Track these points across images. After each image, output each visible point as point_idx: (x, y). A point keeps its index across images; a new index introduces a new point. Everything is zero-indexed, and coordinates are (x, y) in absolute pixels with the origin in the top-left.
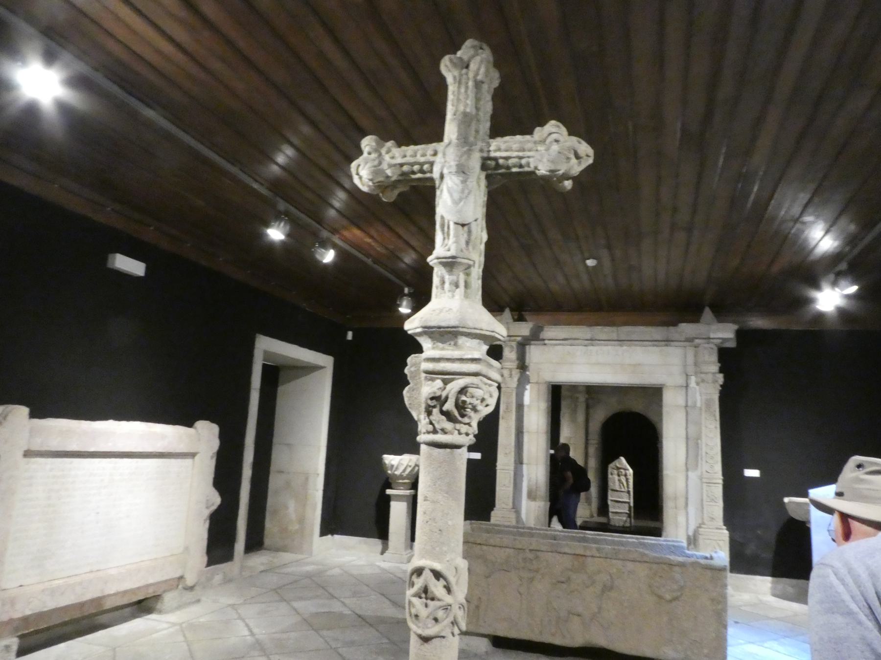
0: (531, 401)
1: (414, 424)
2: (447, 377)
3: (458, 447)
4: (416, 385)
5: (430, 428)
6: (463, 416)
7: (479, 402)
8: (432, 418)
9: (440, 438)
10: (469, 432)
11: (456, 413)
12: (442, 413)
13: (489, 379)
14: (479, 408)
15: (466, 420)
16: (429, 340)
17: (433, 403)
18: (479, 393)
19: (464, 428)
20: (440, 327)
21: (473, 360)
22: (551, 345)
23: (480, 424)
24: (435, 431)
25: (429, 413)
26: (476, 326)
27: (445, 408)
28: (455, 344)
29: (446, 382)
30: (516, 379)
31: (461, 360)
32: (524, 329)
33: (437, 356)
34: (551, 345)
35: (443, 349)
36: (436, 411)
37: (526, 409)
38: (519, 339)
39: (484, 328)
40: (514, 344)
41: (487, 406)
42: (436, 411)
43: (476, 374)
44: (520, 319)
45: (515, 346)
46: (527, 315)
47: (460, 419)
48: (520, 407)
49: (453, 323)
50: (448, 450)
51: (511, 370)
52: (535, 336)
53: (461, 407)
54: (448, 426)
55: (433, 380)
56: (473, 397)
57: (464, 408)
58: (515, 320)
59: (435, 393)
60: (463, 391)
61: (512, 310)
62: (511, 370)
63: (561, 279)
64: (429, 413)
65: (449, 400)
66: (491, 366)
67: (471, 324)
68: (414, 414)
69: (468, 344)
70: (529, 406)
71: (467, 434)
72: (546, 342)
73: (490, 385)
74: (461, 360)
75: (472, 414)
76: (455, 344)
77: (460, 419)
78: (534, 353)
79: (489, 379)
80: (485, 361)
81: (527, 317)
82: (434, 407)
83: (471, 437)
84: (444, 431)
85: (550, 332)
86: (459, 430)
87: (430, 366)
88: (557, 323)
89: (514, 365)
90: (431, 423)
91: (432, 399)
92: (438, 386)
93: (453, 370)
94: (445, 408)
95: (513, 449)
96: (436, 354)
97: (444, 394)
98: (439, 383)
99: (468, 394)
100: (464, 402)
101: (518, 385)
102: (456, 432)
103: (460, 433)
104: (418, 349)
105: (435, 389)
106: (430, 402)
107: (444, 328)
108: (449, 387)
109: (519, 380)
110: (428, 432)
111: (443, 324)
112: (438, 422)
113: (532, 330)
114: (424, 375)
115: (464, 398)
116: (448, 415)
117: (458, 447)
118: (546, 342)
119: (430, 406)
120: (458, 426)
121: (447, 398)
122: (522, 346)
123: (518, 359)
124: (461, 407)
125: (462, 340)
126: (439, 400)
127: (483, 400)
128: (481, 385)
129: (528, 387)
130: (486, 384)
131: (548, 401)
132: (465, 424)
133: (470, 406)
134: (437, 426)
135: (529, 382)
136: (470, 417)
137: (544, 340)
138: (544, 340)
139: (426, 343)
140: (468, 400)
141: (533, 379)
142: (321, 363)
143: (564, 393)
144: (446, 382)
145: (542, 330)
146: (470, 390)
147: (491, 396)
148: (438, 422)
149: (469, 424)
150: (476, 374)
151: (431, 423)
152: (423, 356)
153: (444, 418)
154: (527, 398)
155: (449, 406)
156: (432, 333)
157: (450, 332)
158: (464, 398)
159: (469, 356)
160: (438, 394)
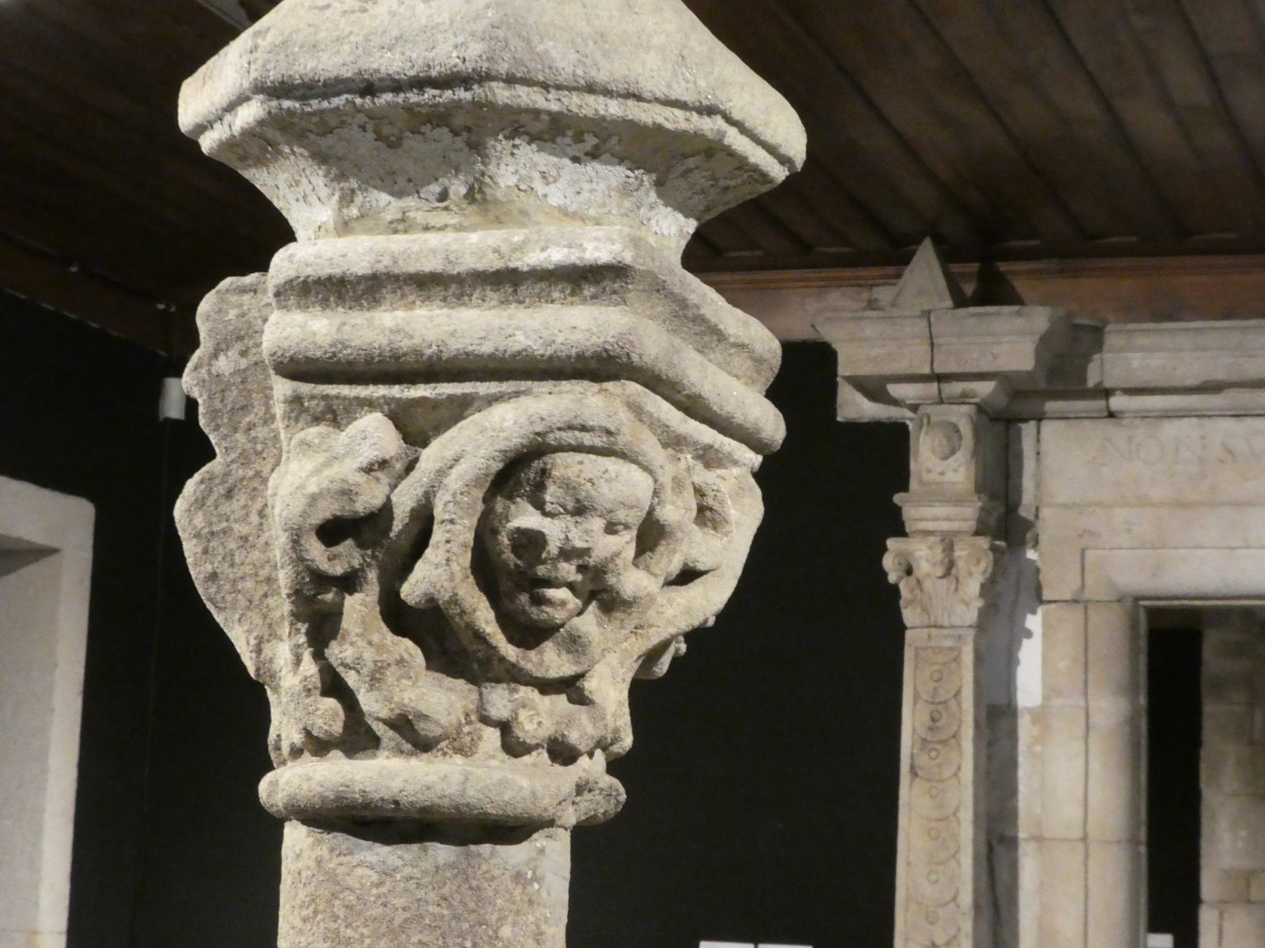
0: (1050, 691)
1: (248, 699)
2: (419, 391)
3: (510, 830)
4: (245, 459)
5: (328, 714)
6: (530, 634)
7: (625, 543)
8: (337, 652)
9: (387, 774)
10: (574, 737)
11: (485, 618)
12: (398, 617)
13: (694, 407)
14: (633, 581)
15: (551, 660)
16: (317, 179)
17: (347, 556)
18: (621, 485)
19: (540, 715)
20: (369, 88)
21: (582, 279)
22: (1144, 415)
23: (643, 693)
24: (357, 737)
25: (321, 627)
26: (601, 76)
27: (412, 590)
28: (476, 195)
29: (416, 428)
30: (973, 587)
31: (507, 282)
32: (1008, 341)
33: (361, 266)
34: (1144, 415)
35: (402, 225)
36: (359, 608)
37: (1026, 729)
38: (985, 389)
39: (653, 84)
40: (961, 416)
41: (688, 576)
42: (359, 608)
43: (599, 367)
44: (994, 292)
45: (966, 429)
46: (1017, 273)
47: (510, 652)
48: (997, 717)
49: (446, 55)
50: (442, 852)
51: (948, 542)
52: (1064, 376)
53: (509, 572)
54: (441, 699)
55: (335, 416)
56: (580, 510)
57: (536, 585)
58: (960, 301)
59: (347, 493)
60: (518, 472)
61: (948, 255)
62: (948, 542)
63: (1187, 84)
64: (321, 627)
65: (438, 535)
66: (709, 335)
67: (565, 63)
68: (241, 639)
69: (556, 195)
70: (1039, 716)
71: (562, 753)
72: (1117, 402)
73: (709, 457)
74: (507, 282)
75: (589, 623)
76: (476, 195)
77: (510, 652)
78: (1064, 462)
79: (694, 407)
80: (658, 288)
81: (1021, 286)
82: (349, 583)
83: (593, 767)
84: (413, 735)
85: (1138, 354)
86: (505, 728)
87: (315, 329)
88: (1167, 310)
89: (966, 515)
90: (333, 685)
91: (331, 532)
92: (368, 454)
93: (455, 346)
94: (412, 590)
95: (967, 926)
96: (359, 253)
97: (405, 500)
98: (373, 434)
99: (552, 494)
100: (530, 542)
101: (982, 626)
102: (492, 737)
103: (513, 747)
104: (257, 234)
105: (348, 470)
106: (316, 551)
107: (397, 86)
108: (431, 457)
109: (987, 589)
110: (318, 746)
111: (393, 63)
112: (375, 680)
113: (1044, 342)
114: (282, 388)
115: (526, 518)
116: (437, 636)
117: (510, 830)
118: (1117, 402)
119: (321, 580)
120: (500, 700)
121: (423, 521)
122: (1002, 428)
123: (981, 487)
124: (509, 572)
125: (514, 166)
126: (370, 537)
127: (651, 535)
128: (631, 433)
129: (1034, 622)
130: (674, 442)
131: (1133, 688)
132: (547, 687)
133: (568, 570)
134: (369, 702)
135: (1039, 599)
136: (575, 644)
137: (1107, 393)
138: (1107, 393)
139: (301, 195)
140: (555, 531)
141: (1059, 582)
142: (31, 531)
143: (1215, 658)
144: (416, 428)
145: (1098, 345)
146: (565, 465)
147: (706, 515)
148: (375, 680)
149: (571, 687)
150: (599, 367)
151: (333, 685)
152: (284, 263)
153: (407, 648)
154: (1029, 684)
155: (439, 573)
156: (326, 125)
157: (439, 117)
158: (526, 518)
159: (557, 256)
160: (370, 497)
